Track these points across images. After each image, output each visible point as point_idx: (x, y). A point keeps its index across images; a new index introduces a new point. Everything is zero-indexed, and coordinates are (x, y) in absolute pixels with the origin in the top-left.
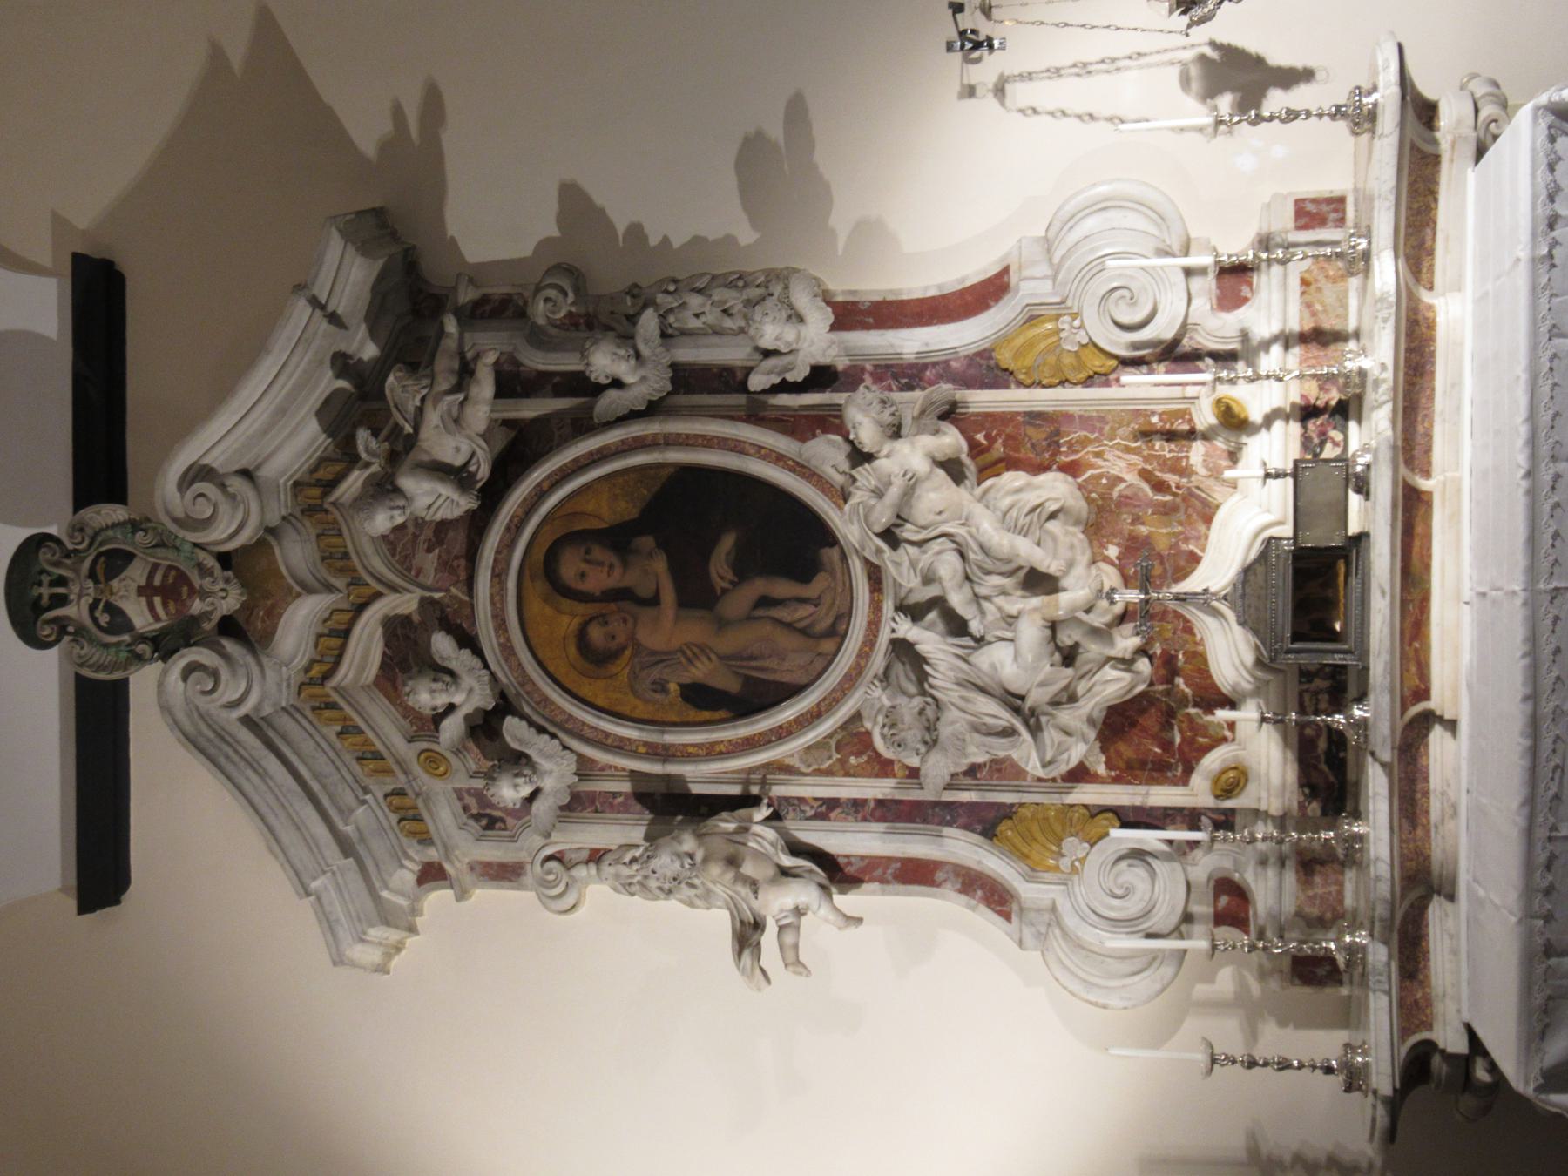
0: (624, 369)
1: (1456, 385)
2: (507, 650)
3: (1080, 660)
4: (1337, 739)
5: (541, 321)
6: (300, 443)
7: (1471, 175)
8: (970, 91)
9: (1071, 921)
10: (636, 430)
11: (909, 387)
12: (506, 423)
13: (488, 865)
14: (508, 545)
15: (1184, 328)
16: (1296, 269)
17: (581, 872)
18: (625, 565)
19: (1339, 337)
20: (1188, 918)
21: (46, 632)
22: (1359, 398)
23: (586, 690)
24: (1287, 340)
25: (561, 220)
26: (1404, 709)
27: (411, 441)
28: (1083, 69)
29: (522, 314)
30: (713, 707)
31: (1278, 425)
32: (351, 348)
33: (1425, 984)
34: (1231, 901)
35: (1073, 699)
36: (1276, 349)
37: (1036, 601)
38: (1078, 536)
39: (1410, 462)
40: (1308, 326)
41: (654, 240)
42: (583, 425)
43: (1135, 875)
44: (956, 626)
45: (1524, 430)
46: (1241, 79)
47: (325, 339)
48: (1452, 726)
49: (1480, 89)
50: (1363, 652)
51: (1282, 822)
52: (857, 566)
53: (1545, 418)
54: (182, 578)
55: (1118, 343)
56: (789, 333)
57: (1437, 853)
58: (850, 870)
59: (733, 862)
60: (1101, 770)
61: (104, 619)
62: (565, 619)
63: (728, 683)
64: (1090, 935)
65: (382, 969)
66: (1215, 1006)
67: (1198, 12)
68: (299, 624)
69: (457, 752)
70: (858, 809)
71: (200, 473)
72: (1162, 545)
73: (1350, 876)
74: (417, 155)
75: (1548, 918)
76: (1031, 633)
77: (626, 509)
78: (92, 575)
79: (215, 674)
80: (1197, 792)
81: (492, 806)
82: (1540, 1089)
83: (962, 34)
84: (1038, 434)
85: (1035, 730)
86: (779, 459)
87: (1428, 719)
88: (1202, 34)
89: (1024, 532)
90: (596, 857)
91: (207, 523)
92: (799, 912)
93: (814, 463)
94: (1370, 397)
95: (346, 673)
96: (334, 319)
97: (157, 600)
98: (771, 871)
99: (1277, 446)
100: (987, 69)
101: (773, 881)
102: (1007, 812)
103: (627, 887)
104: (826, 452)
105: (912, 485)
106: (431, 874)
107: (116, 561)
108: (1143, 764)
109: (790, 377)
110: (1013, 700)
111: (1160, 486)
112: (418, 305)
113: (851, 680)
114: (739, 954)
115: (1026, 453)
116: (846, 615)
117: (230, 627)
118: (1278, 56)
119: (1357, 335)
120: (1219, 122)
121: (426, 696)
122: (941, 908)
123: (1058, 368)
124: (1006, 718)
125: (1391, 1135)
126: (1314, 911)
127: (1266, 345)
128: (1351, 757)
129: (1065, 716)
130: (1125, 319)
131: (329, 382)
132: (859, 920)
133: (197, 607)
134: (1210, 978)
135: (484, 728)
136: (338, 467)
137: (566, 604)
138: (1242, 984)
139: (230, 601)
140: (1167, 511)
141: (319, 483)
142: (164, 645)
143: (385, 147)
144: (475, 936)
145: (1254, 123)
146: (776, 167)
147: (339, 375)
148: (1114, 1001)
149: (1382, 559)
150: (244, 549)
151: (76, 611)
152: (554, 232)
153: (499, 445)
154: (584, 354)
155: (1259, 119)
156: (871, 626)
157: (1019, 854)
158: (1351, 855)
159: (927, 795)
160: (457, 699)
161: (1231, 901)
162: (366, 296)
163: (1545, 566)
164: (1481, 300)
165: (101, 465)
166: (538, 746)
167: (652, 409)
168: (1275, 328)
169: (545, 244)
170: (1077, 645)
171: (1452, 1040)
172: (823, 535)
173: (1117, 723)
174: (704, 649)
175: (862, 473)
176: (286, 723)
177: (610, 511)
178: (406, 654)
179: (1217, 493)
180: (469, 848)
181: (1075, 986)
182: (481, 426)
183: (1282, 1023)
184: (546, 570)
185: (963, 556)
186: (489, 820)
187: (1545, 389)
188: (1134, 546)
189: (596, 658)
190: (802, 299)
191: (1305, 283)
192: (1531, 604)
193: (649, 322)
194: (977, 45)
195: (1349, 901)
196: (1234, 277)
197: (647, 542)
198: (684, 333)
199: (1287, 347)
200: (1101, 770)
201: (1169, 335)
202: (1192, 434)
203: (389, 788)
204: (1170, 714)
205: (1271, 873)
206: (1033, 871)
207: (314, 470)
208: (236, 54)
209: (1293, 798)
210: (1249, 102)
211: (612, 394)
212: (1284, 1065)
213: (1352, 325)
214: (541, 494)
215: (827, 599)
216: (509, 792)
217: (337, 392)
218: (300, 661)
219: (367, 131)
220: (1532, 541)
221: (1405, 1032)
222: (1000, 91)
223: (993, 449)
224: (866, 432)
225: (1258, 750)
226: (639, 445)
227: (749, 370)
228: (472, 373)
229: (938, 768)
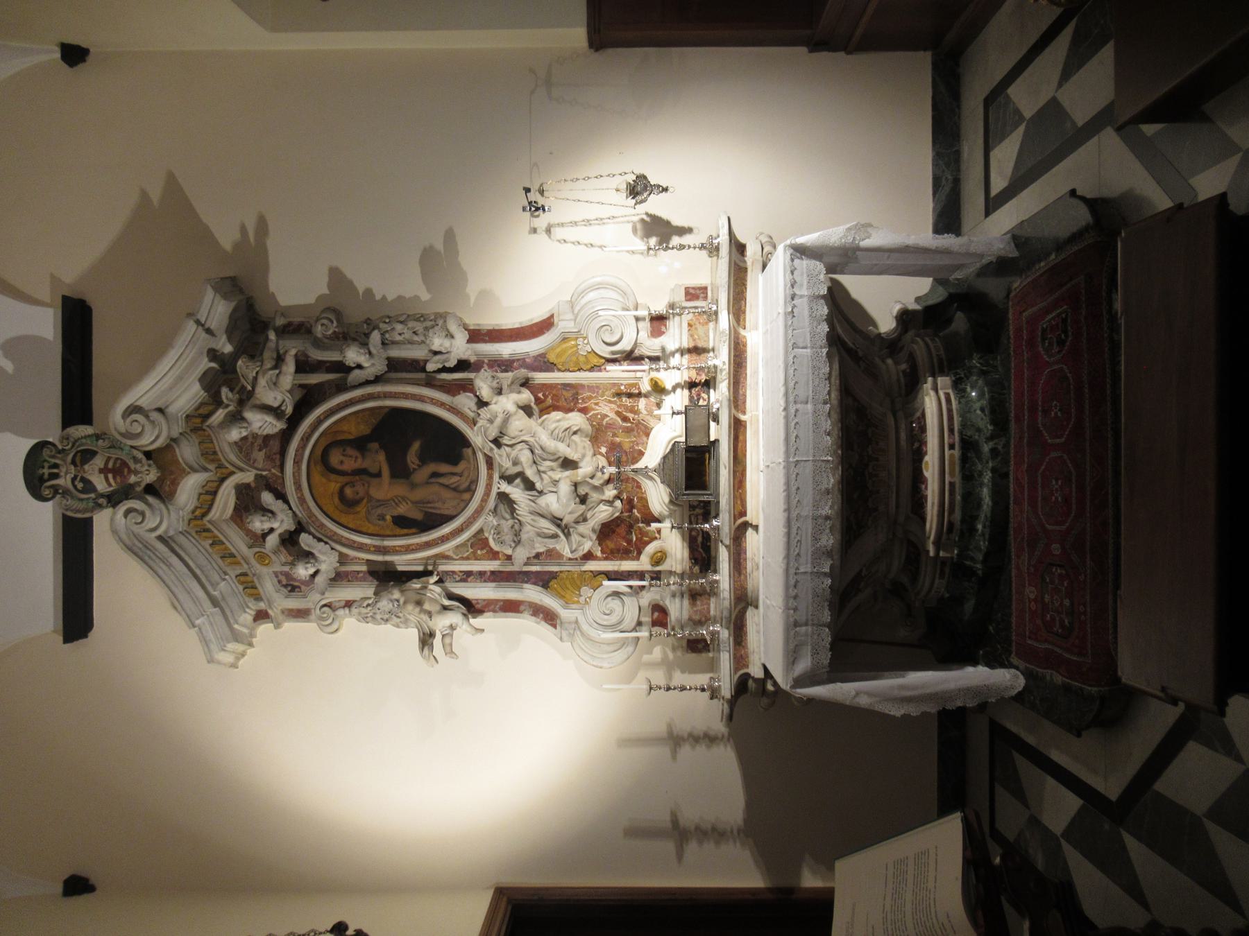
0: (363, 359)
6: (189, 395)
24: (682, 352)
34: (659, 615)
42: (341, 387)
43: (615, 604)
44: (529, 486)
55: (605, 351)
63: (418, 516)
64: (593, 633)
68: (189, 488)
70: (481, 576)
71: (134, 409)
74: (254, 250)
76: (565, 488)
77: (364, 429)
80: (644, 563)
87: (746, 525)
90: (349, 604)
95: (214, 514)
99: (679, 400)
100: (542, 221)
104: (465, 402)
106: (261, 616)
110: (556, 521)
112: (253, 326)
116: (475, 482)
117: (150, 489)
118: (677, 221)
121: (258, 524)
122: (524, 623)
129: (584, 528)
131: (205, 364)
135: (290, 540)
139: (151, 475)
140: (628, 431)
143: (237, 246)
146: (440, 263)
156: (487, 486)
161: (659, 615)
166: (318, 548)
167: (378, 380)
169: (320, 298)
172: (464, 442)
173: (606, 531)
177: (356, 430)
179: (651, 422)
184: (322, 459)
186: (292, 587)
188: (613, 447)
189: (349, 504)
190: (453, 327)
193: (375, 337)
196: (658, 320)
206: (567, 604)
208: (155, 195)
214: (319, 422)
216: (303, 571)
219: (227, 239)
223: (546, 401)
224: (485, 392)
226: (371, 397)
229: (521, 555)
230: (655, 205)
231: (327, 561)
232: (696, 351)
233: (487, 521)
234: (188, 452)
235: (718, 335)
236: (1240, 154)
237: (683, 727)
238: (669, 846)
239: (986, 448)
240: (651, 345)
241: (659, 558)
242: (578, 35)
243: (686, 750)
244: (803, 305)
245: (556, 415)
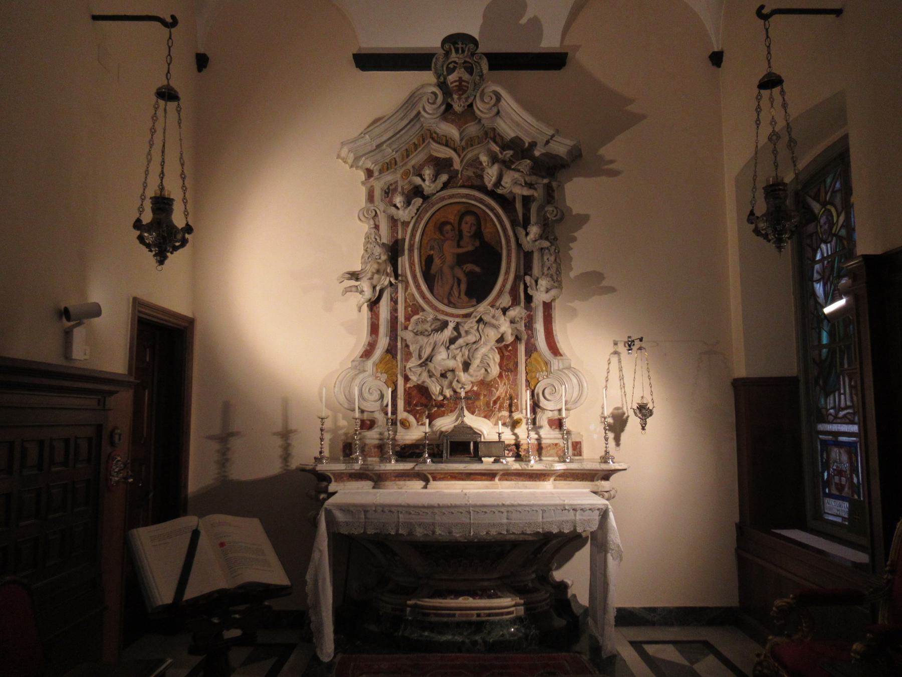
0: (531, 236)
1: (526, 488)
2: (443, 199)
3: (443, 380)
4: (420, 455)
5: (546, 209)
6: (508, 130)
7: (588, 490)
8: (616, 344)
9: (361, 376)
10: (513, 240)
11: (525, 326)
12: (514, 198)
13: (373, 192)
14: (476, 199)
15: (543, 409)
16: (561, 443)
17: (372, 222)
18: (471, 237)
19: (540, 455)
20: (362, 411)
21: (447, 46)
22: (522, 460)
23: (430, 224)
24: (539, 440)
25: (578, 215)
26: (431, 474)
27: (509, 168)
28: (622, 378)
29: (549, 202)
30: (426, 265)
31: (514, 437)
32: (538, 148)
33: (348, 480)
34: (368, 424)
35: (430, 377)
36: (536, 436)
37: (461, 365)
38: (480, 378)
39: (504, 475)
40: (543, 446)
41: (571, 245)
42: (514, 223)
43: (376, 395)
44: (452, 341)
45: (516, 503)
46: (617, 425)
47: (541, 140)
48: (425, 487)
49: (612, 493)
50: (446, 462)
51: (394, 439)
52: (471, 310)
53: (519, 509)
54: (465, 92)
55: (539, 389)
56: (543, 289)
57: (387, 483)
58: (375, 308)
59: (378, 272)
60: (408, 385)
61: (451, 66)
62: (453, 217)
63: (433, 270)
64: (357, 381)
65: (338, 157)
66: (335, 419)
67: (638, 411)
68: (451, 130)
69: (410, 182)
70: (394, 310)
71: (498, 97)
72: (477, 403)
73: (377, 459)
74: (600, 168)
75: (375, 511)
76: (451, 364)
77: (487, 237)
78: (465, 62)
79: (434, 103)
80: (402, 414)
81: (393, 194)
82: (326, 510)
83: (633, 341)
84: (511, 366)
85: (421, 365)
86: (504, 286)
87: (427, 481)
88: (631, 413)
89: (481, 362)
90: (377, 227)
91: (483, 101)
92: (362, 292)
93: (502, 297)
94: (523, 463)
95: (434, 145)
96: (548, 142)
97: (457, 83)
98: (375, 283)
99: (508, 437)
100: (622, 349)
101: (372, 284)
102: (394, 356)
103: (367, 237)
104: (506, 300)
105: (496, 327)
106: (369, 173)
107: (470, 70)
108: (410, 398)
109: (529, 289)
110: (430, 358)
111: (495, 402)
112: (551, 169)
113: (435, 308)
114: (349, 273)
115: (505, 362)
116: (455, 307)
117: (449, 107)
118: (624, 436)
119: (540, 460)
120: (605, 418)
121: (428, 172)
123: (531, 371)
124: (425, 356)
125: (303, 470)
126: (366, 449)
127: (538, 433)
128: (413, 459)
130: (546, 391)
131: (527, 140)
132: (360, 311)
133: (455, 97)
134: (344, 418)
135: (417, 191)
136: (500, 143)
137: (458, 218)
138: (341, 428)
139: (458, 107)
140: (488, 404)
141: (495, 136)
142: (442, 85)
144: (352, 187)
145: (604, 428)
146: (594, 284)
147: (529, 143)
148: (336, 389)
149: (475, 467)
150: (473, 113)
151: (454, 56)
152: (574, 213)
153: (508, 196)
154: (536, 223)
155: (605, 430)
157: (381, 360)
158: (384, 458)
159: (399, 332)
160: (427, 183)
161: (368, 424)
162: (554, 153)
163: (477, 509)
164: (551, 493)
165: (502, 62)
166: (413, 209)
167: (519, 245)
168: (543, 436)
169: (570, 209)
170: (446, 377)
171: (332, 487)
172: (480, 299)
173: (423, 390)
174: (444, 262)
175: (499, 312)
176: (418, 126)
177: (487, 231)
179: (493, 420)
180: (378, 186)
181: (341, 377)
182: (514, 191)
183: (330, 440)
184: (469, 211)
185: (474, 343)
186: (388, 192)
187: (527, 509)
188: (477, 395)
189: (440, 227)
190: (553, 292)
191: (556, 444)
192: (466, 506)
193: (546, 244)
194: (630, 346)
195: (369, 459)
196: (559, 424)
197: (477, 244)
198: (542, 255)
199: (537, 439)
200: (408, 385)
201: (541, 405)
202: (511, 412)
203: (398, 160)
204: (426, 406)
205: (378, 436)
206: (376, 365)
207: (499, 134)
209: (401, 442)
210: (611, 428)
211: (524, 233)
212: (322, 440)
213: (544, 458)
215: (460, 301)
216: (398, 200)
217: (524, 143)
218: (438, 130)
219: (607, 151)
220: (484, 506)
221: (334, 474)
222: (616, 353)
223: (507, 352)
224: (512, 313)
225: (415, 433)
227: (531, 276)
228: (530, 188)
229: (408, 335)
230: (634, 422)
231: (404, 214)
234: (472, 129)
237: (295, 441)
238: (216, 431)
239: (478, 638)
240: (543, 419)
242: (741, 371)
244: (570, 516)
245: (497, 358)
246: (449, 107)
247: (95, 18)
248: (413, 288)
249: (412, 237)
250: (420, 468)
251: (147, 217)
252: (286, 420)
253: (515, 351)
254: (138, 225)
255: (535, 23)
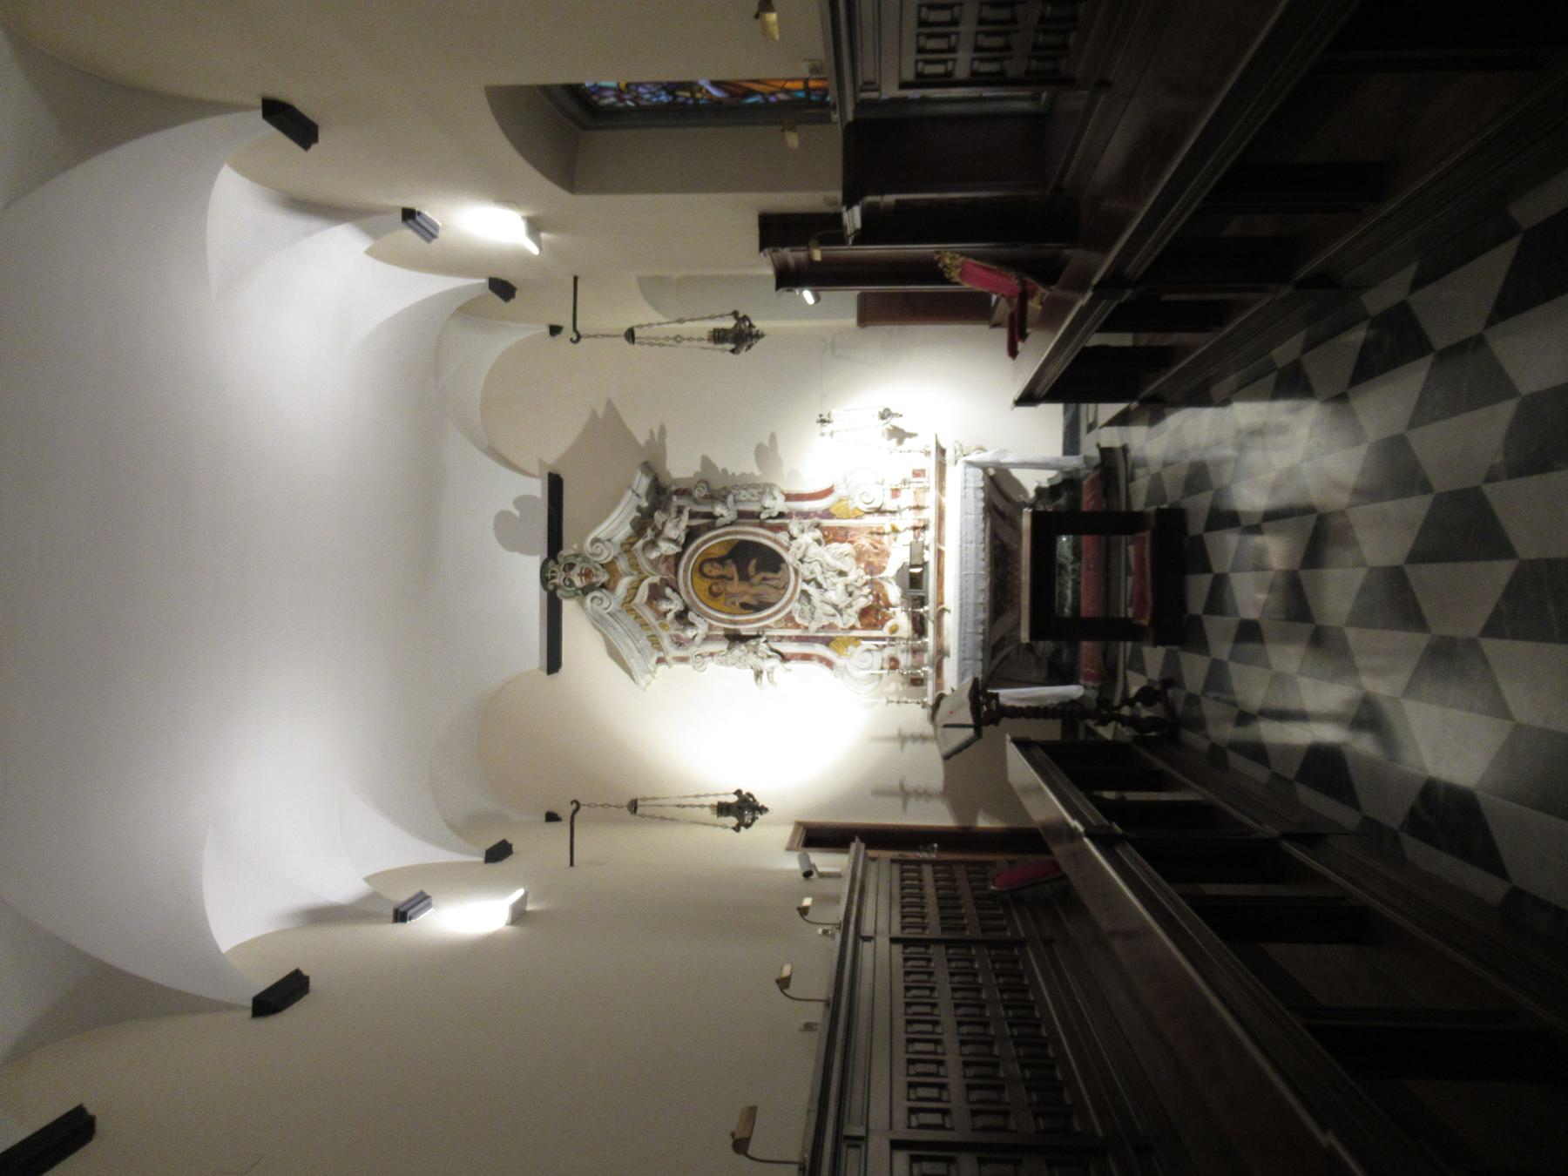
0: (724, 512)
6: (626, 530)
24: (910, 508)
34: (894, 663)
42: (711, 527)
43: (868, 655)
44: (819, 586)
46: (899, 435)
55: (865, 508)
63: (753, 602)
70: (790, 638)
71: (596, 540)
76: (840, 587)
77: (723, 552)
80: (885, 632)
87: (943, 610)
90: (712, 654)
95: (637, 600)
100: (828, 428)
104: (783, 537)
106: (660, 661)
107: (571, 566)
110: (835, 606)
112: (661, 493)
117: (603, 586)
118: (907, 430)
121: (664, 606)
122: (814, 667)
124: (833, 611)
129: (850, 611)
131: (635, 514)
135: (681, 616)
139: (603, 577)
143: (648, 443)
146: (765, 453)
149: (932, 568)
154: (1089, 677)
156: (795, 586)
157: (836, 651)
161: (894, 663)
167: (732, 523)
172: (781, 560)
173: (864, 613)
178: (656, 594)
179: (891, 550)
184: (700, 570)
186: (679, 643)
188: (869, 564)
189: (714, 595)
190: (776, 493)
193: (730, 498)
196: (895, 492)
204: (878, 611)
206: (840, 655)
214: (698, 547)
216: (690, 633)
219: (642, 438)
223: (831, 536)
224: (795, 530)
229: (814, 626)
230: (895, 422)
231: (702, 628)
232: (918, 508)
233: (795, 606)
234: (622, 565)
235: (930, 499)
236: (1513, 245)
237: (907, 731)
238: (898, 801)
240: (890, 504)
241: (894, 630)
242: (852, 321)
243: (909, 745)
244: (970, 492)
245: (835, 545)
246: (603, 586)
247: (572, 864)
248: (770, 622)
249: (723, 621)
250: (932, 616)
251: (732, 820)
252: (890, 739)
253: (829, 528)
254: (737, 829)
255: (519, 502)
